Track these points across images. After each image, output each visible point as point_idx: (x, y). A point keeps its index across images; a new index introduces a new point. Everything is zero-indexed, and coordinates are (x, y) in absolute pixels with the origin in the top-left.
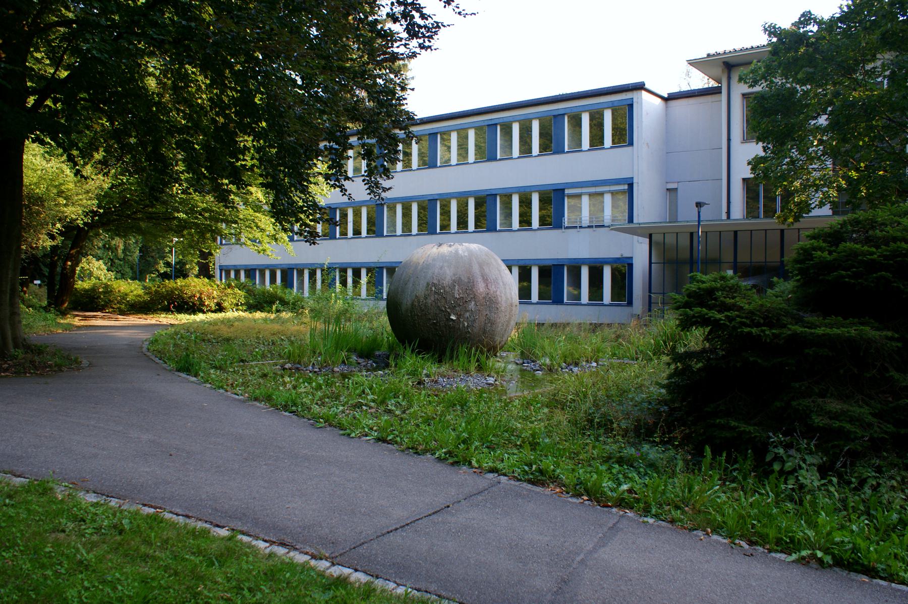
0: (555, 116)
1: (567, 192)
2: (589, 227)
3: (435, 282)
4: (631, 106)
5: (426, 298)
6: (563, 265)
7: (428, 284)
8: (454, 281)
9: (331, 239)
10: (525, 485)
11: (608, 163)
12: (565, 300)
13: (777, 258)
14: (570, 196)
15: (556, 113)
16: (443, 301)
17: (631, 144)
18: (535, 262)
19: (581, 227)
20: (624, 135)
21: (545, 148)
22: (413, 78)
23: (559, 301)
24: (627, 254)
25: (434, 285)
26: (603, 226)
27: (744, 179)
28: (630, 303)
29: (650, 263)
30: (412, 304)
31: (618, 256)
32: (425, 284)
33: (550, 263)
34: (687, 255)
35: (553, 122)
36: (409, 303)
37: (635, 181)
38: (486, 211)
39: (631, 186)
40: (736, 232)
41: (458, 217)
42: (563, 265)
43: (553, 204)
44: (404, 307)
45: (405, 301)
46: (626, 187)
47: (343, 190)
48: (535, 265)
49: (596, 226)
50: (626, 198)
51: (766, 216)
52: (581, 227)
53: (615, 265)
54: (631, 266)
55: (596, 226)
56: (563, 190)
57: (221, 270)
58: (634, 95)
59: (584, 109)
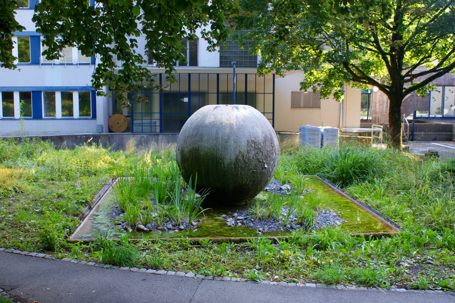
3: (253, 139)
5: (248, 153)
6: (41, 91)
7: (248, 142)
10: (412, 290)
12: (43, 117)
18: (16, 88)
23: (38, 116)
25: (253, 142)
26: (72, 64)
28: (94, 117)
30: (237, 159)
31: (85, 85)
32: (246, 142)
33: (30, 90)
36: (233, 157)
40: (189, 74)
42: (41, 91)
44: (227, 161)
45: (228, 157)
48: (17, 91)
49: (67, 64)
51: (191, 65)
53: (80, 91)
55: (67, 64)
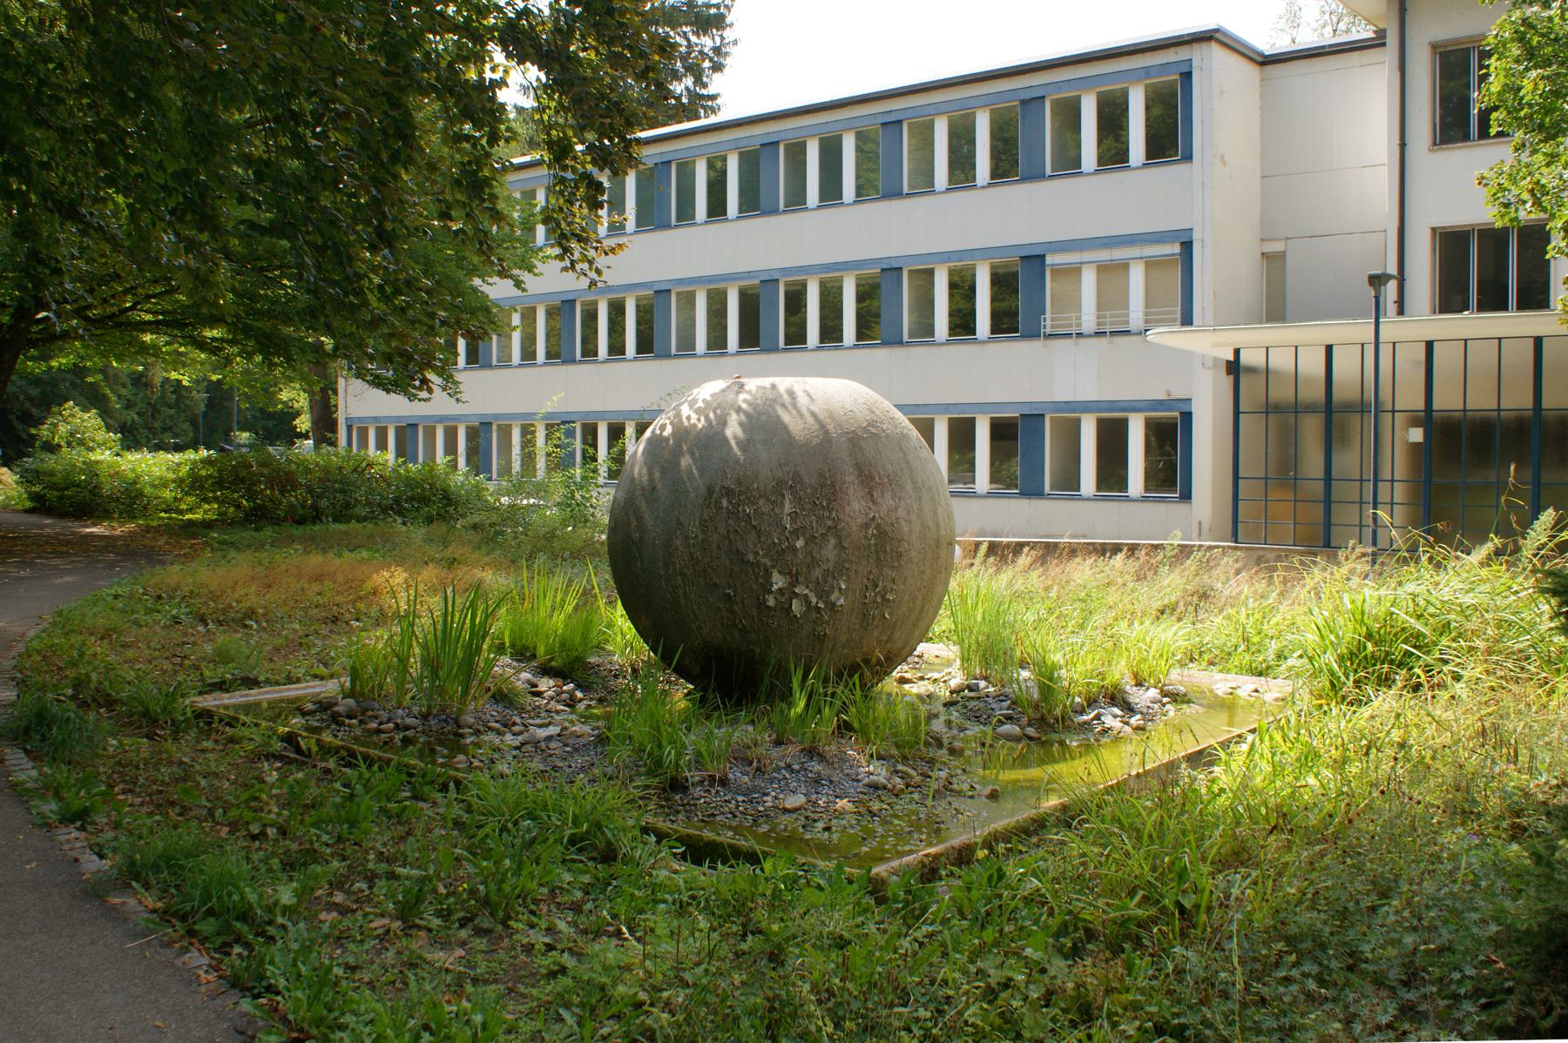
0: (1023, 102)
1: (1049, 260)
2: (1098, 334)
4: (1187, 76)
8: (780, 483)
9: (564, 362)
11: (1137, 198)
13: (1528, 402)
14: (1059, 271)
15: (1027, 95)
16: (752, 537)
17: (1188, 157)
19: (1080, 335)
20: (1168, 140)
21: (646, 345)
22: (735, 42)
23: (1033, 491)
24: (1178, 394)
27: (1434, 230)
28: (1186, 496)
29: (1237, 413)
34: (1319, 394)
35: (1024, 121)
37: (1196, 236)
38: (878, 309)
39: (1187, 246)
41: (823, 318)
43: (1016, 297)
46: (1177, 249)
47: (518, 284)
50: (1335, 474)
52: (1080, 335)
54: (1187, 417)
56: (1042, 257)
57: (349, 428)
58: (1196, 54)
59: (1086, 83)
